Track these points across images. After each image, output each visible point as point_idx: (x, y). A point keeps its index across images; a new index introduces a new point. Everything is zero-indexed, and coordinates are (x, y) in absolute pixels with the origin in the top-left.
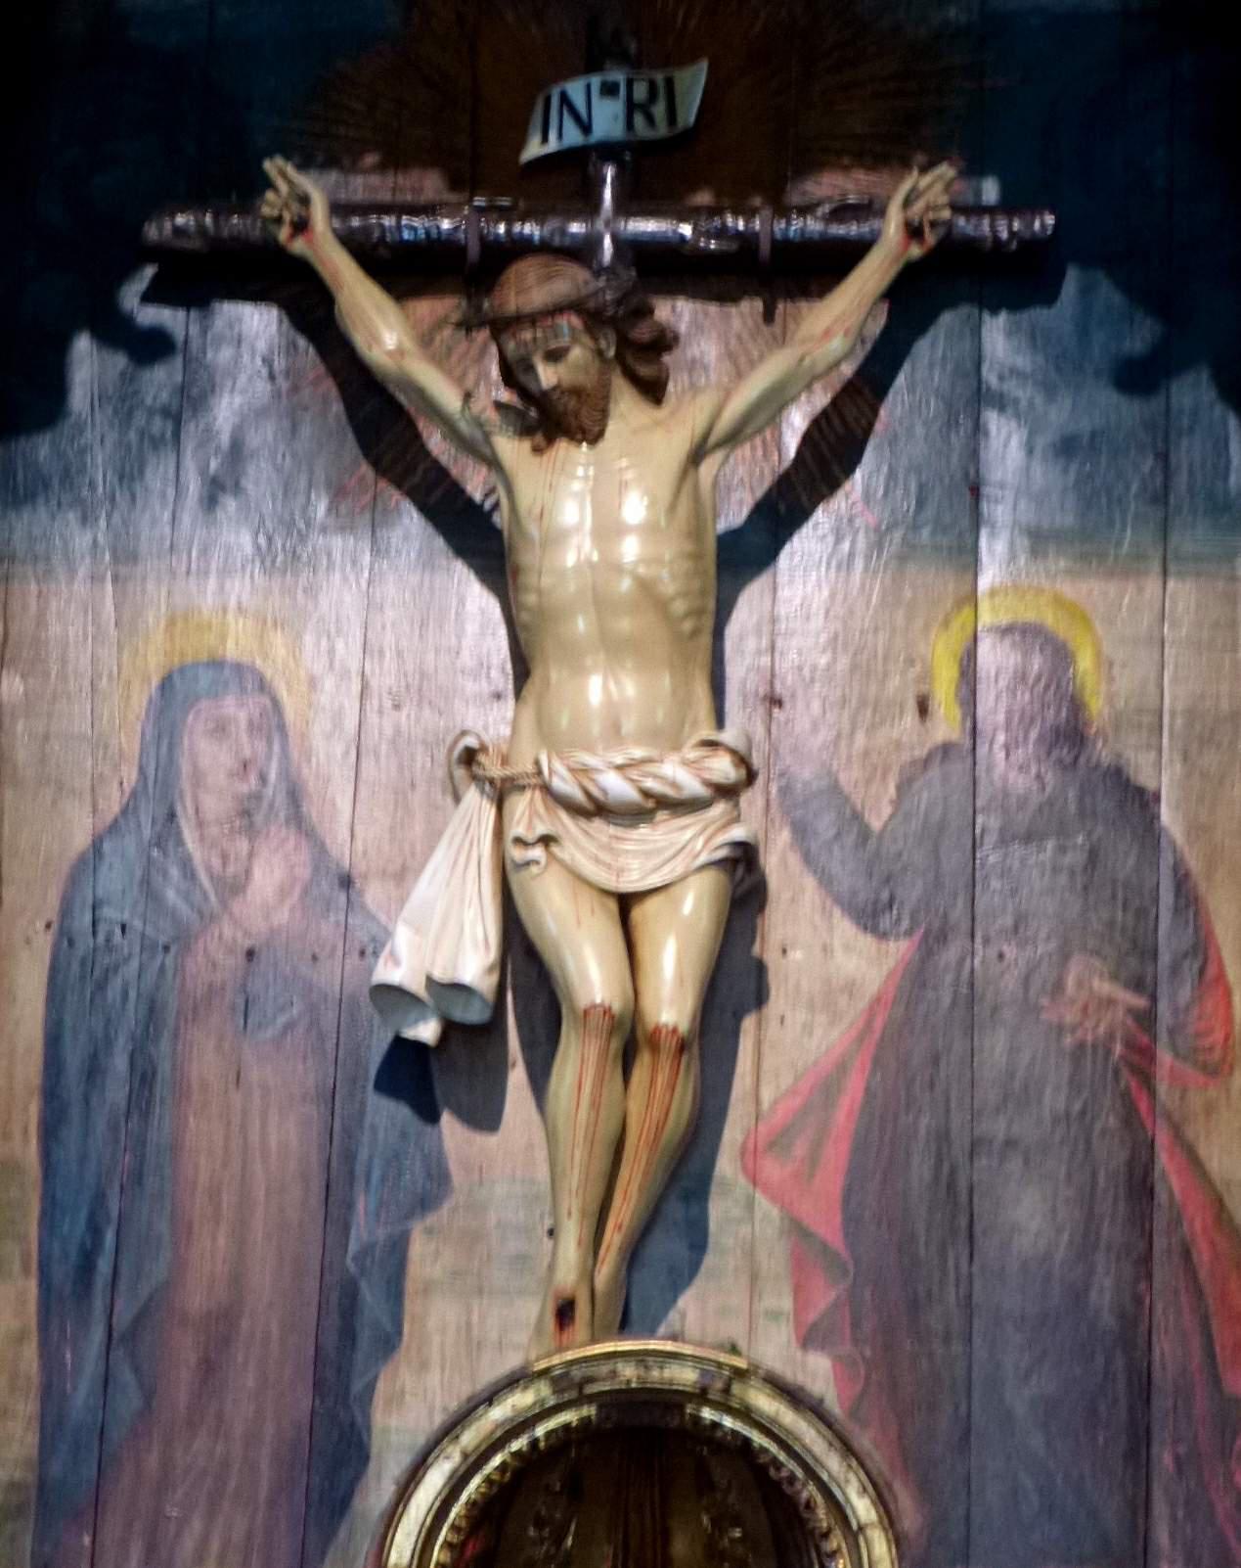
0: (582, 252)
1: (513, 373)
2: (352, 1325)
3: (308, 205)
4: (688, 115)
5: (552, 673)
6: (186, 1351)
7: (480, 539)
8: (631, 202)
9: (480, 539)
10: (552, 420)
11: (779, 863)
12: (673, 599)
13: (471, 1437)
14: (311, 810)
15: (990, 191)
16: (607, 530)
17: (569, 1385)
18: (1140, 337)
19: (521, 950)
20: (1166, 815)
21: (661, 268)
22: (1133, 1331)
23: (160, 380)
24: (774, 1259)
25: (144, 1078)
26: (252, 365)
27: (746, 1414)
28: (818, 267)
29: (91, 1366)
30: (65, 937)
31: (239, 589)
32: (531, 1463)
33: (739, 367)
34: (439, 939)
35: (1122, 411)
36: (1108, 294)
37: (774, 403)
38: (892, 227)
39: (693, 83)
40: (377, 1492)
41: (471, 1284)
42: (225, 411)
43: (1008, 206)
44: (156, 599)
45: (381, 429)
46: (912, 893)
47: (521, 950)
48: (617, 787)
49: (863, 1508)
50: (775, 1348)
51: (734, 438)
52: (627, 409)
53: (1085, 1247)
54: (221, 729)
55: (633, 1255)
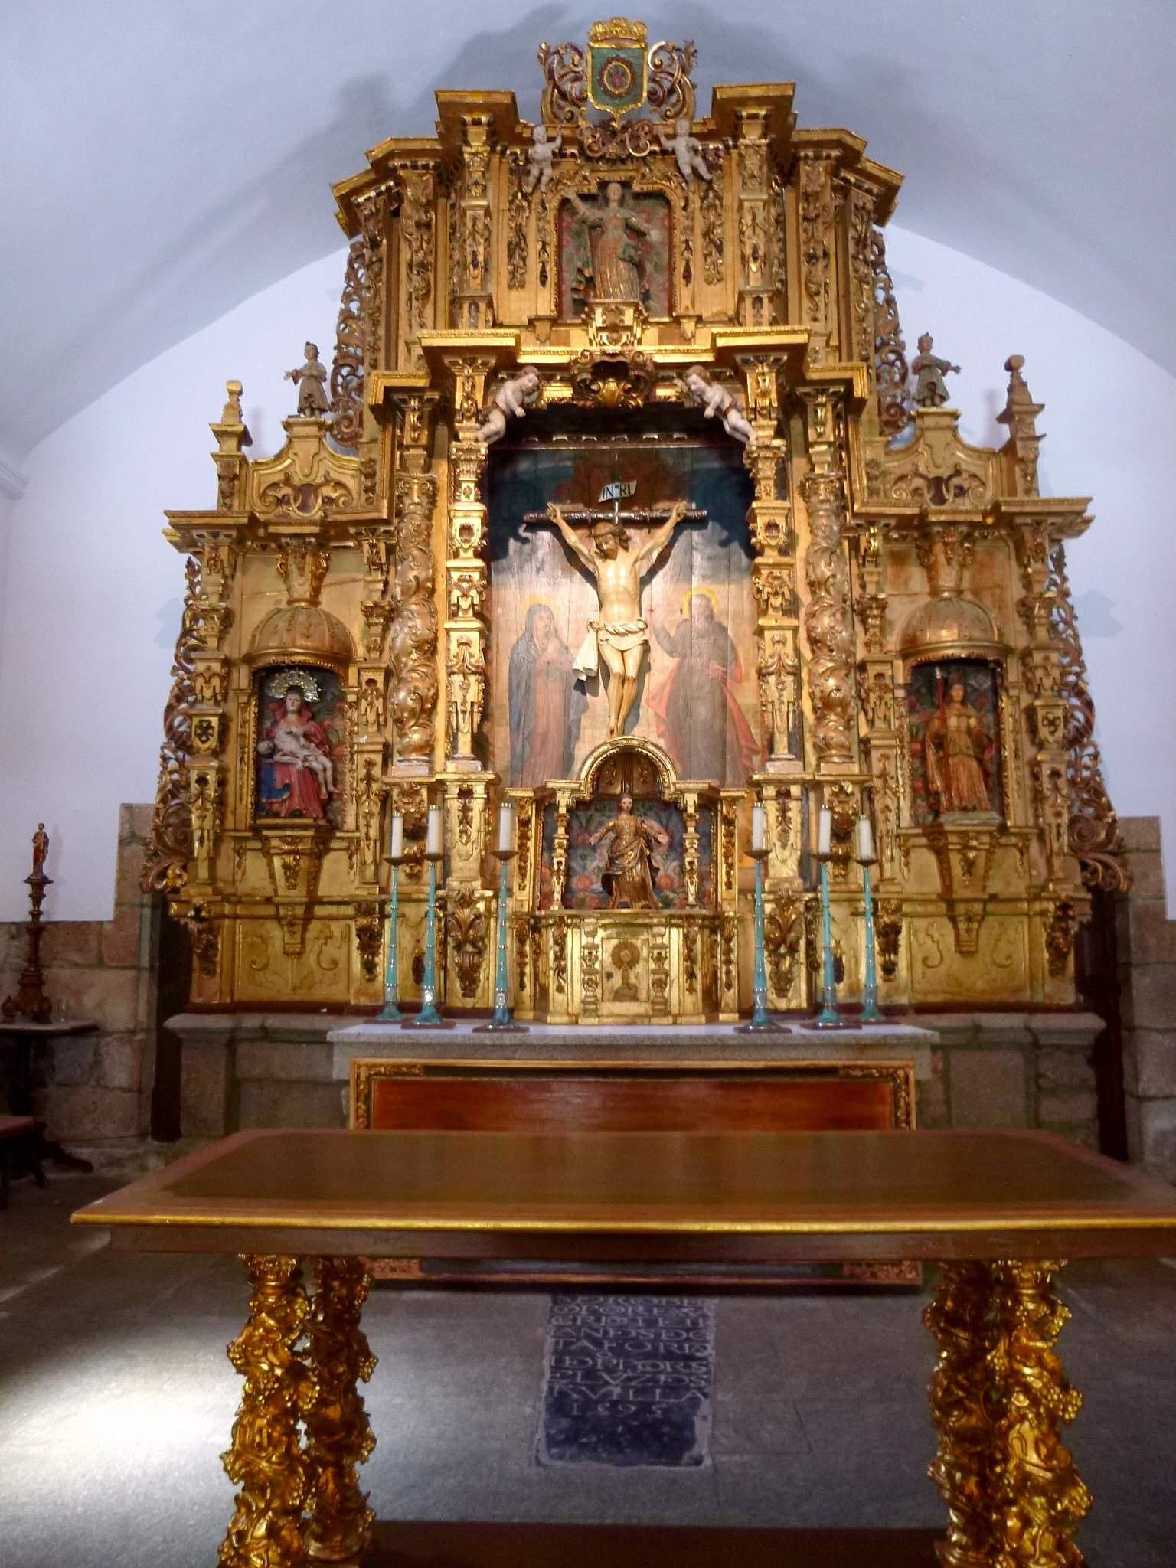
0: (610, 521)
2: (570, 736)
3: (556, 511)
4: (633, 491)
5: (606, 606)
6: (538, 743)
7: (591, 578)
8: (621, 509)
9: (591, 578)
10: (606, 555)
11: (653, 644)
12: (771, 799)
13: (595, 755)
15: (694, 506)
16: (617, 577)
17: (614, 745)
18: (725, 534)
19: (602, 661)
21: (627, 523)
22: (723, 732)
23: (527, 547)
24: (653, 721)
25: (528, 687)
26: (545, 544)
28: (659, 522)
30: (511, 659)
31: (544, 590)
32: (607, 760)
33: (643, 542)
34: (585, 660)
35: (722, 551)
36: (718, 527)
37: (650, 552)
38: (674, 514)
39: (633, 485)
40: (576, 767)
41: (593, 727)
42: (540, 554)
43: (698, 509)
44: (527, 592)
45: (571, 555)
46: (679, 648)
47: (602, 661)
48: (621, 630)
49: (669, 766)
50: (653, 738)
51: (643, 558)
52: (621, 552)
53: (714, 716)
54: (541, 618)
55: (625, 721)
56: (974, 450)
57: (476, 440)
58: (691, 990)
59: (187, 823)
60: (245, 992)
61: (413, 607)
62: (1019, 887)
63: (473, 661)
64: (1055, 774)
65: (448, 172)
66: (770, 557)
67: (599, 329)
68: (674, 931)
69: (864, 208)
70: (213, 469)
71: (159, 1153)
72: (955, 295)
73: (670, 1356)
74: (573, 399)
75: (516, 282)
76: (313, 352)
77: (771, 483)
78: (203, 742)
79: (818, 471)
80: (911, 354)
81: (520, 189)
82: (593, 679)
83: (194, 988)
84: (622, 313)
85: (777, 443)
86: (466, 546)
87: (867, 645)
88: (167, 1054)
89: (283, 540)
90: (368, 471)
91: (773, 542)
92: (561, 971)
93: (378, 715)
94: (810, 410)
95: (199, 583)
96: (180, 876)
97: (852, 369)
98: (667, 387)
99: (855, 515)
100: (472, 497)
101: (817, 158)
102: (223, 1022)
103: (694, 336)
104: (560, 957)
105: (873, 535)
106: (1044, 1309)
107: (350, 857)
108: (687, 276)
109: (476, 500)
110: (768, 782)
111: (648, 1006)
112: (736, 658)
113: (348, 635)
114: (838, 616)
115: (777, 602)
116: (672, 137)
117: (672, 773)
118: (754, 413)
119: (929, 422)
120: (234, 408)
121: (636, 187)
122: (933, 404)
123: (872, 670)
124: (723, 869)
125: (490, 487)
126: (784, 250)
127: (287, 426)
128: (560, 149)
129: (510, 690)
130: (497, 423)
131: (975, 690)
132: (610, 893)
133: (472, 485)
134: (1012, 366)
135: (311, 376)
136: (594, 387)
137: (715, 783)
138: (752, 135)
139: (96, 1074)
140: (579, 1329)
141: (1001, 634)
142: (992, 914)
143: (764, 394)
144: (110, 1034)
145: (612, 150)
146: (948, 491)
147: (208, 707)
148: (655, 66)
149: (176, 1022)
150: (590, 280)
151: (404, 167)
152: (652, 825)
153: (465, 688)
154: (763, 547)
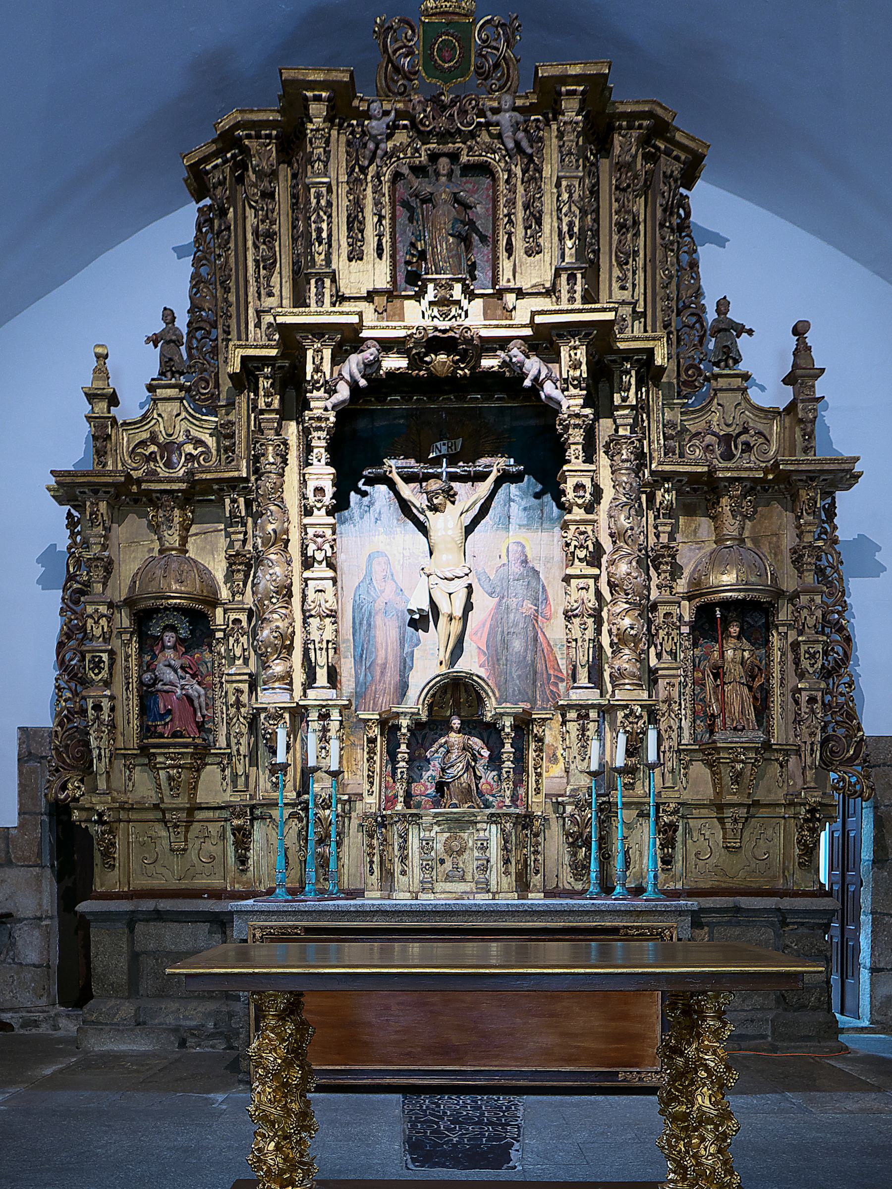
0: (438, 476)
1: (430, 500)
2: (405, 666)
7: (423, 528)
9: (423, 528)
10: (435, 509)
13: (431, 684)
14: (395, 578)
18: (539, 487)
20: (541, 576)
21: (453, 477)
23: (366, 500)
24: (475, 652)
27: (473, 680)
28: (481, 477)
29: (363, 674)
37: (474, 503)
42: (377, 505)
45: (405, 507)
46: (498, 590)
48: (450, 576)
53: (526, 650)
55: (452, 653)
56: (761, 410)
57: (326, 409)
58: (507, 873)
59: (87, 743)
60: (140, 882)
61: (272, 557)
62: (779, 796)
63: (328, 605)
64: (812, 700)
65: (291, 142)
66: (578, 513)
67: (431, 303)
68: (494, 827)
69: (671, 176)
70: (86, 429)
71: (68, 1016)
72: (755, 261)
73: (490, 1123)
74: (408, 368)
75: (356, 255)
76: (169, 316)
77: (580, 447)
78: (96, 675)
79: (621, 432)
80: (711, 315)
81: (357, 163)
82: (424, 618)
83: (97, 880)
84: (451, 288)
85: (588, 411)
86: (319, 505)
87: (659, 587)
88: (75, 933)
89: (154, 495)
90: (224, 433)
91: (580, 501)
92: (404, 859)
93: (244, 650)
94: (617, 374)
95: (79, 533)
96: (79, 788)
97: (654, 339)
98: (490, 357)
99: (652, 473)
100: (323, 461)
101: (630, 127)
102: (125, 906)
103: (514, 308)
104: (403, 848)
105: (667, 491)
106: (719, 1024)
107: (223, 770)
108: (510, 249)
109: (327, 464)
110: (571, 707)
111: (473, 885)
112: (546, 599)
113: (213, 579)
114: (634, 563)
115: (582, 554)
116: (496, 111)
117: (493, 699)
118: (565, 384)
119: (722, 383)
120: (101, 372)
121: (464, 159)
122: (727, 366)
123: (662, 610)
124: (533, 778)
125: (337, 455)
126: (597, 220)
127: (151, 388)
128: (394, 122)
129: (354, 628)
130: (343, 392)
131: (752, 626)
132: (442, 796)
133: (323, 450)
134: (800, 330)
135: (168, 342)
136: (427, 359)
137: (527, 706)
138: (571, 111)
139: (11, 953)
140: (425, 1111)
141: (774, 578)
142: (753, 817)
143: (576, 366)
144: (20, 920)
145: (442, 123)
146: (736, 448)
147: (99, 644)
148: (484, 41)
149: (83, 907)
150: (422, 255)
151: (248, 137)
152: (476, 743)
153: (321, 629)
154: (571, 505)
